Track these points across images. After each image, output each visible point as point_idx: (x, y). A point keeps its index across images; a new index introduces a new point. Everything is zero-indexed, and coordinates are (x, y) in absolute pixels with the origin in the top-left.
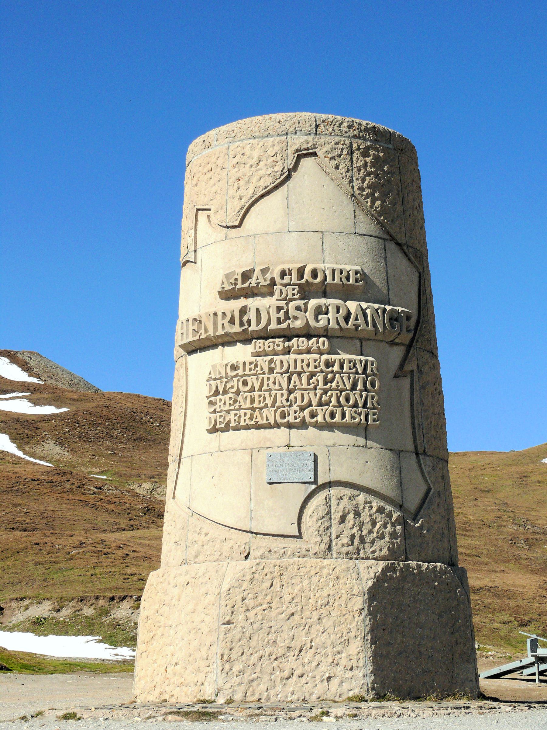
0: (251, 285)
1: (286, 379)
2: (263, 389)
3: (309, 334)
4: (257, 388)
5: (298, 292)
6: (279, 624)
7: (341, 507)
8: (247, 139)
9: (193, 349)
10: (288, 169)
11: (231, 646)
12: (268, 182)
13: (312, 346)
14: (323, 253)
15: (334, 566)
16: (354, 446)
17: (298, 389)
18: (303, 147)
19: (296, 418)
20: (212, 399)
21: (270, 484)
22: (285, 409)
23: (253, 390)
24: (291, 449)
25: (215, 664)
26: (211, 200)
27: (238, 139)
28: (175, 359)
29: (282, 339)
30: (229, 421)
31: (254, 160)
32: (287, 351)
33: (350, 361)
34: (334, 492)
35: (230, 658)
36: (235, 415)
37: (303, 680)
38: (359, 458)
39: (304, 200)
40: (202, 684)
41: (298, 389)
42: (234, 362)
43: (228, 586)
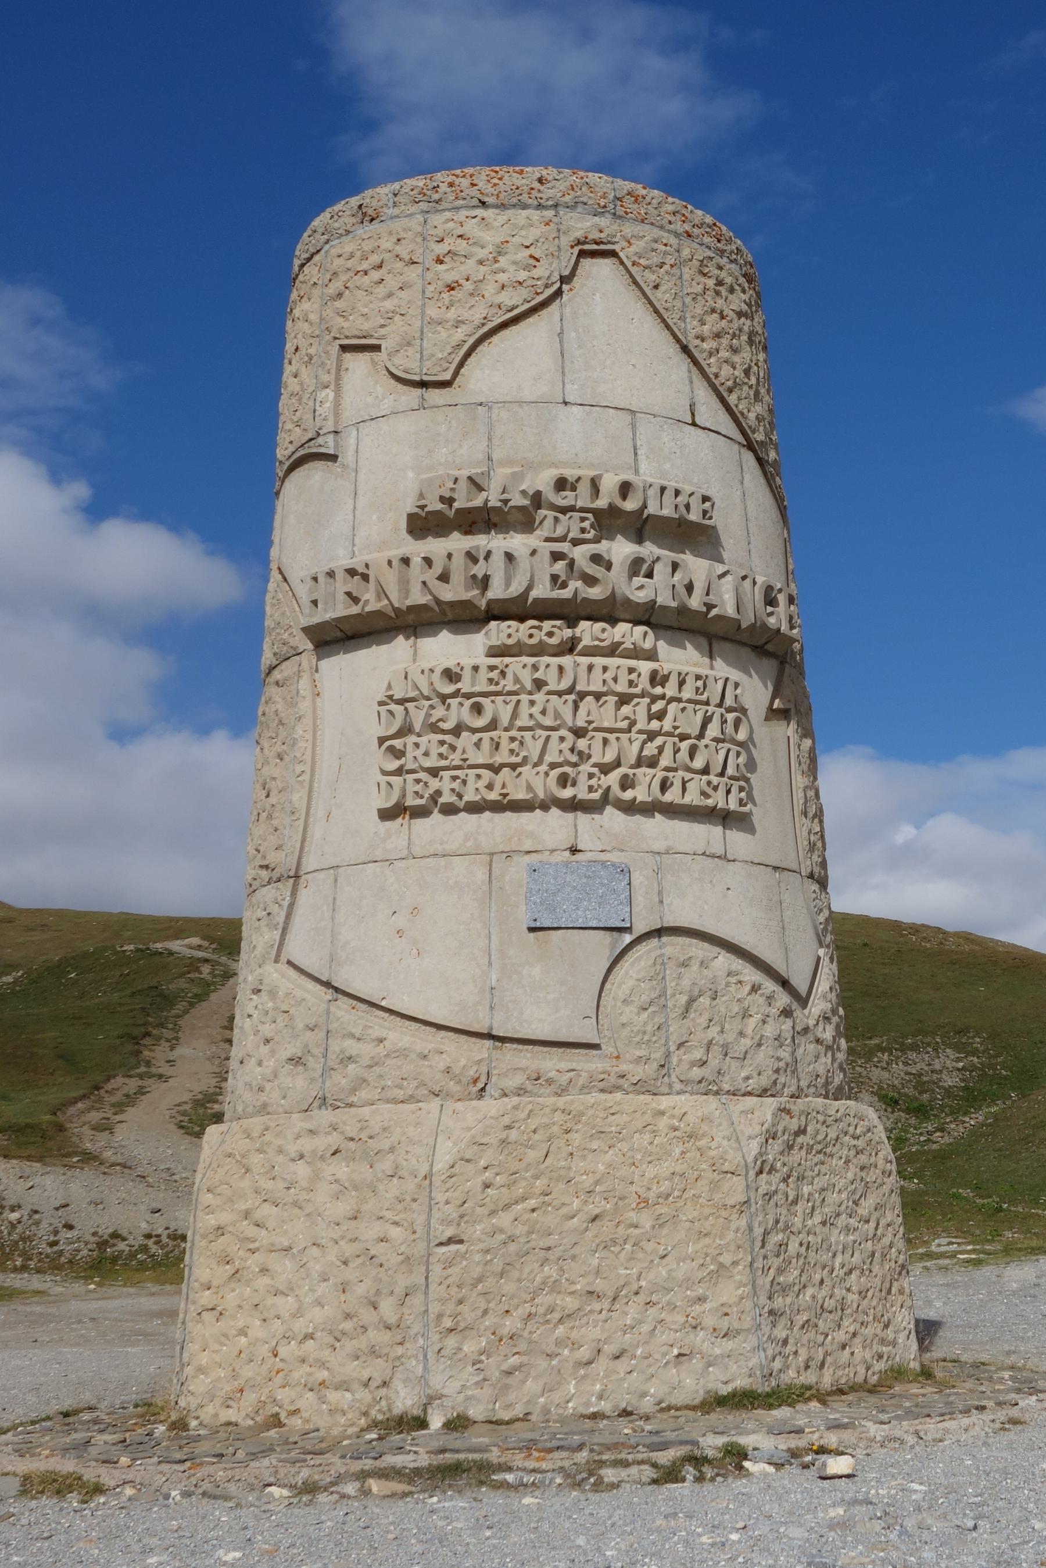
0: (490, 504)
1: (570, 704)
2: (519, 723)
3: (611, 616)
4: (505, 720)
5: (592, 526)
6: (567, 1241)
7: (686, 982)
8: (467, 207)
9: (335, 637)
10: (561, 277)
11: (460, 1296)
12: (516, 299)
13: (622, 640)
14: (636, 454)
15: (683, 1111)
16: (704, 854)
17: (596, 730)
18: (591, 237)
19: (591, 789)
20: (397, 743)
21: (532, 930)
22: (568, 769)
23: (493, 725)
24: (579, 857)
25: (419, 1336)
26: (382, 326)
27: (450, 206)
28: (267, 658)
29: (558, 623)
30: (438, 793)
31: (486, 251)
32: (570, 647)
33: (698, 677)
34: (673, 946)
35: (458, 1323)
36: (454, 778)
37: (622, 1366)
38: (714, 881)
39: (595, 343)
40: (385, 1384)
41: (596, 730)
42: (451, 664)
43: (448, 1159)
